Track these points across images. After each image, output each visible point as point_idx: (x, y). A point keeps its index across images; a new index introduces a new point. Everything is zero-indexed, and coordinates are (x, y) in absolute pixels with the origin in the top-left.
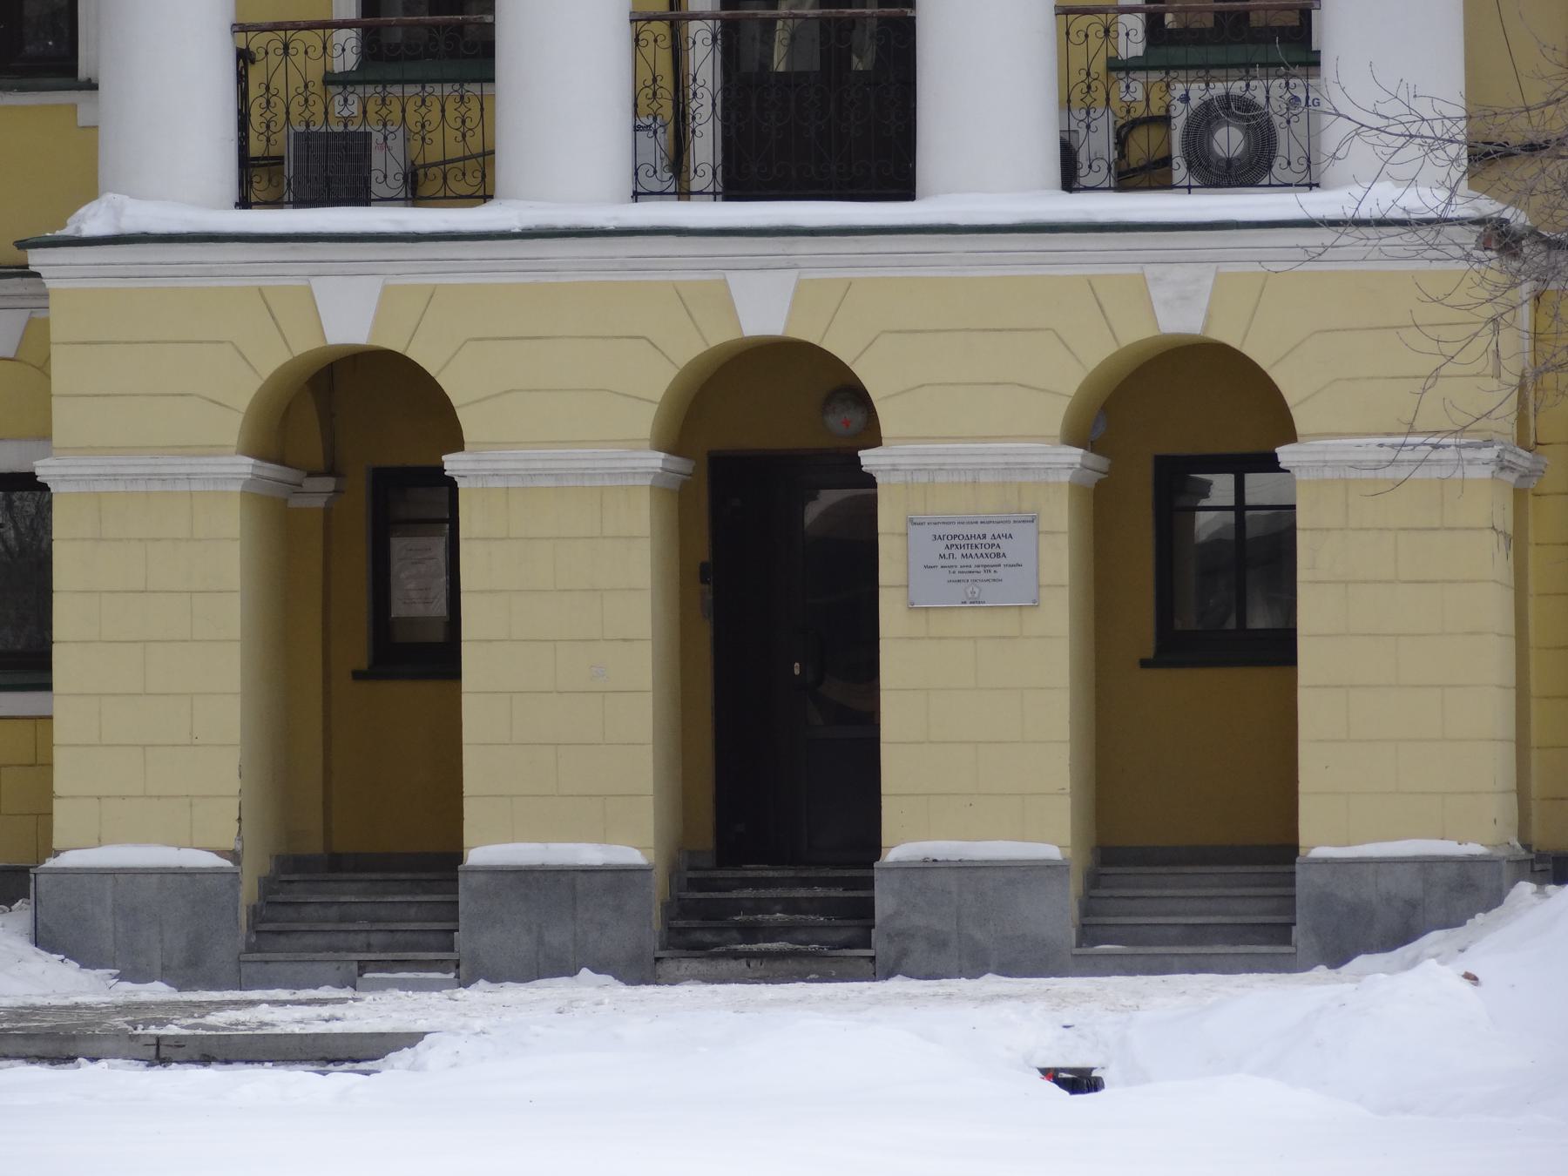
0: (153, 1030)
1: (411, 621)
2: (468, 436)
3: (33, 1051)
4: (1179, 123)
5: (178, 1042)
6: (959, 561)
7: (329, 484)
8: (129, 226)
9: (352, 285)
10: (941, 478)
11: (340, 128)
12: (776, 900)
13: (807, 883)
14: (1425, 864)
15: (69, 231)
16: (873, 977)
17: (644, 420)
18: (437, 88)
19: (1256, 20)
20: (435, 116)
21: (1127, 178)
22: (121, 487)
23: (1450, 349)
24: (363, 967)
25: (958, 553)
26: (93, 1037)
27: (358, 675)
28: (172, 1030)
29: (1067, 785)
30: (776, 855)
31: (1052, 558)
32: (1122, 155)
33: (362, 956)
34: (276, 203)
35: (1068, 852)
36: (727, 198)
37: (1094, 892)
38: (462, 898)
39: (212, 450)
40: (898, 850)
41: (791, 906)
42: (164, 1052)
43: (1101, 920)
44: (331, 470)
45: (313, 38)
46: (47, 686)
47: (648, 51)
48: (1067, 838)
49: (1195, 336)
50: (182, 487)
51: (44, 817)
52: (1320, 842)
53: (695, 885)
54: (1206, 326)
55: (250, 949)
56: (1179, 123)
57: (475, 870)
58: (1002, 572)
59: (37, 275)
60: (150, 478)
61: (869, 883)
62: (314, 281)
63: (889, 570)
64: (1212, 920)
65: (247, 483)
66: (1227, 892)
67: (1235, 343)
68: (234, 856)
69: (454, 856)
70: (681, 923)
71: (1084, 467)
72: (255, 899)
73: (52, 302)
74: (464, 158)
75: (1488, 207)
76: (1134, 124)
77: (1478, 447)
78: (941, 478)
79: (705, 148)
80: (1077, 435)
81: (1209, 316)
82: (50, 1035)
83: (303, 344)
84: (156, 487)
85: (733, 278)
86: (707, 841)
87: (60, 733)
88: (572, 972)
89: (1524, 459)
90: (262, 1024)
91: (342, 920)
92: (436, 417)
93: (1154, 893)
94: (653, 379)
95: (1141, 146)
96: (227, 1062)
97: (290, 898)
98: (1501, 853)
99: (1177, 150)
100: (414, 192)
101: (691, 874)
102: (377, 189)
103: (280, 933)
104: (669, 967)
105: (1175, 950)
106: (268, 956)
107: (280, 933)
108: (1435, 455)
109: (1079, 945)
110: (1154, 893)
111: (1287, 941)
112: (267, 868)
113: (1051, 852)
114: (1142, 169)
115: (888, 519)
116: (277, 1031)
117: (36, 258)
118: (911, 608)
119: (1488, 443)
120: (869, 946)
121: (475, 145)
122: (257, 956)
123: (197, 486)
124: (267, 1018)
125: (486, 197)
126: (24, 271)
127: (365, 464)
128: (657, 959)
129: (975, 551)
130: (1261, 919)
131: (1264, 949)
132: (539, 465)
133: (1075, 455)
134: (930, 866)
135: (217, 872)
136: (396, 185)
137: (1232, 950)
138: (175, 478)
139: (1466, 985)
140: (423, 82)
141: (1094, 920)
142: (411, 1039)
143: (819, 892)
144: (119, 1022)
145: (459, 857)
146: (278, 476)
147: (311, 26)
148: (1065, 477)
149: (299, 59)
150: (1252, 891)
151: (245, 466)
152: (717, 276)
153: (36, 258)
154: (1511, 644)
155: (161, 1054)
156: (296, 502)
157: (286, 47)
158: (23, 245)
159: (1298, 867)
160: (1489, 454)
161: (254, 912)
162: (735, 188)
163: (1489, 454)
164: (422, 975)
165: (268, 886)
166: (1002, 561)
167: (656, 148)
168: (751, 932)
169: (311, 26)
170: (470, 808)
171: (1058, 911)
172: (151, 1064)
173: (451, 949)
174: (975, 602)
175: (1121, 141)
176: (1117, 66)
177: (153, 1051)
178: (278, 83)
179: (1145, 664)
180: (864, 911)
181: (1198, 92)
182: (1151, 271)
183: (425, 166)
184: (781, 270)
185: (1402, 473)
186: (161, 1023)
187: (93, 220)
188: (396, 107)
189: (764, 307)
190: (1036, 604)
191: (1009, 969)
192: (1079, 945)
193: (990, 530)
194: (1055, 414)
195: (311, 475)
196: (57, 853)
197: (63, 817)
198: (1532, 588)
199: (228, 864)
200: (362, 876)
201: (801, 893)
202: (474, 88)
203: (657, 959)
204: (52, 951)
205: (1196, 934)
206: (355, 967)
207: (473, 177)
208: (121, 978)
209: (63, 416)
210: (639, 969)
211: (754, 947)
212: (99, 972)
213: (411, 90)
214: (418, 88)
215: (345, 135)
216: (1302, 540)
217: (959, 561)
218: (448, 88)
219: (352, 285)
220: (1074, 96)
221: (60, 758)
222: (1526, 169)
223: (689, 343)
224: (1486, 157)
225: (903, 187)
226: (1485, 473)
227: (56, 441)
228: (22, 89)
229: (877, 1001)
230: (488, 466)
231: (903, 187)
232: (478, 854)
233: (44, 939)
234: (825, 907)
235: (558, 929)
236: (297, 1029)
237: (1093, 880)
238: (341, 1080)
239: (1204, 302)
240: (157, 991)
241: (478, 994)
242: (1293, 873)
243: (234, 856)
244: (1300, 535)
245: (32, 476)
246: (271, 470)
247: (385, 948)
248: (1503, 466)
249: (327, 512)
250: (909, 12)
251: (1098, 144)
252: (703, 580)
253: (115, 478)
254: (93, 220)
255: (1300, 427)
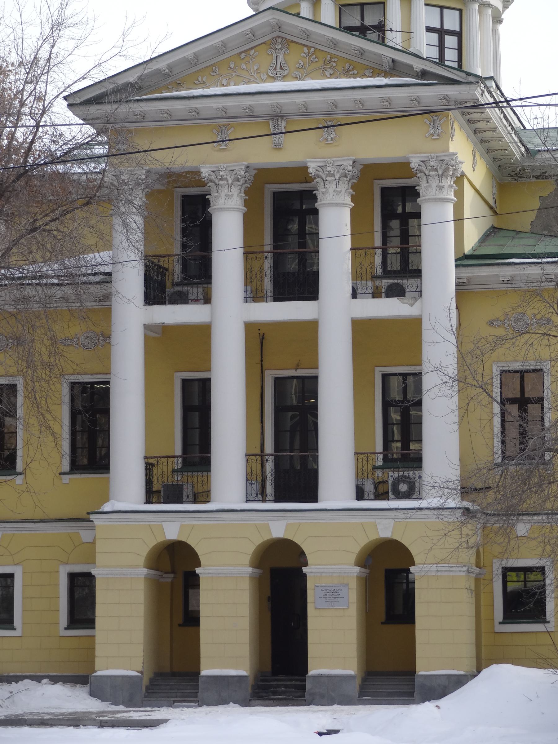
0: (101, 718)
1: (192, 611)
2: (202, 563)
3: (69, 723)
4: (390, 482)
5: (106, 722)
6: (328, 596)
7: (172, 575)
8: (116, 508)
9: (173, 524)
10: (324, 575)
11: (171, 483)
12: (282, 685)
13: (291, 680)
14: (449, 676)
15: (101, 510)
16: (306, 705)
17: (247, 559)
18: (196, 473)
19: (412, 456)
20: (195, 480)
21: (379, 496)
22: (113, 576)
23: (435, 542)
24: (174, 702)
25: (328, 594)
26: (86, 720)
27: (180, 625)
28: (106, 718)
29: (356, 655)
30: (282, 673)
31: (352, 596)
32: (376, 491)
33: (174, 699)
34: (159, 502)
35: (356, 673)
36: (275, 502)
37: (365, 683)
38: (200, 683)
39: (137, 567)
40: (312, 672)
41: (286, 686)
42: (103, 724)
43: (366, 691)
44: (173, 572)
45: (164, 460)
46: (94, 628)
47: (250, 464)
48: (356, 669)
49: (173, 540)
50: (129, 576)
51: (93, 662)
52: (422, 670)
53: (262, 681)
54: (392, 535)
55: (145, 697)
56: (390, 482)
57: (203, 677)
58: (339, 599)
59: (92, 521)
60: (121, 574)
61: (304, 680)
62: (163, 523)
63: (310, 599)
64: (395, 691)
65: (145, 575)
66: (400, 683)
67: (399, 540)
68: (141, 672)
69: (197, 673)
70: (257, 691)
71: (360, 572)
72: (148, 684)
73: (96, 528)
74: (203, 492)
75: (466, 504)
76: (380, 483)
77: (462, 567)
78: (324, 575)
79: (270, 489)
80: (358, 564)
81: (392, 533)
82: (74, 719)
83: (160, 539)
84: (122, 576)
85: (270, 522)
86: (268, 668)
87: (98, 639)
88: (227, 703)
89: (477, 570)
90: (130, 717)
91: (171, 689)
92: (300, 555)
93: (380, 683)
94: (249, 548)
95: (381, 489)
96: (119, 727)
97: (157, 683)
98: (468, 674)
99: (390, 490)
100: (195, 501)
101: (261, 678)
102: (185, 498)
103: (153, 693)
104: (253, 702)
105: (384, 698)
106: (150, 699)
107: (153, 693)
108: (451, 569)
109: (359, 697)
110: (380, 683)
111: (413, 696)
112: (152, 675)
113: (351, 672)
114: (382, 494)
115: (310, 585)
116: (132, 718)
117: (92, 517)
118: (316, 608)
119: (465, 566)
120: (304, 697)
121: (206, 488)
122: (147, 699)
123: (133, 576)
124: (131, 715)
125: (209, 501)
126: (89, 520)
127: (176, 569)
128: (250, 700)
129: (332, 594)
130: (408, 691)
131: (407, 698)
132: (220, 571)
133: (358, 569)
134: (320, 676)
135: (137, 677)
136: (191, 498)
137: (398, 698)
138: (127, 574)
139: (436, 709)
140: (193, 472)
141: (363, 691)
142: (165, 721)
143: (293, 683)
144: (93, 716)
145: (199, 673)
146: (160, 574)
147: (164, 457)
148: (355, 574)
149: (161, 466)
150: (405, 683)
151: (145, 571)
152: (373, 521)
153: (92, 517)
154: (474, 619)
155: (102, 725)
156: (161, 580)
157: (368, 459)
158: (89, 513)
159: (415, 677)
160: (465, 569)
161: (147, 688)
162: (277, 500)
163: (465, 569)
164: (189, 704)
165: (151, 680)
166: (339, 596)
167: (256, 487)
168: (275, 693)
169: (164, 457)
170: (202, 660)
171: (354, 688)
172: (99, 727)
173: (197, 697)
174: (332, 607)
175: (376, 487)
176: (375, 468)
177: (99, 724)
178: (365, 468)
179: (382, 623)
180: (303, 688)
181: (396, 475)
182: (378, 521)
183: (198, 493)
184: (282, 521)
185: (423, 574)
186: (103, 716)
187: (107, 507)
188: (186, 478)
189: (278, 530)
190: (348, 608)
191: (341, 703)
192: (359, 697)
193: (336, 588)
194: (352, 558)
195: (166, 573)
196: (96, 672)
197: (98, 662)
198: (482, 603)
199: (140, 674)
200: (175, 677)
201: (289, 683)
202: (205, 473)
203: (250, 700)
204: (94, 697)
205: (390, 694)
206: (172, 702)
207: (202, 496)
208: (112, 704)
209: (99, 558)
210: (245, 703)
211: (275, 697)
212: (106, 703)
213: (189, 474)
214: (191, 473)
215: (173, 485)
216: (416, 591)
217: (328, 596)
218: (199, 473)
219: (173, 524)
220: (360, 475)
221: (97, 647)
222: (473, 496)
223: (259, 540)
224: (465, 492)
225: (315, 499)
226: (464, 574)
227: (97, 564)
228: (81, 474)
229: (297, 711)
230: (207, 571)
231: (315, 499)
232: (204, 672)
233: (92, 694)
234: (295, 687)
235: (225, 692)
236: (137, 718)
237: (364, 680)
238: (146, 732)
239: (391, 528)
240: (121, 708)
241: (205, 709)
242: (414, 679)
243: (141, 672)
244: (416, 590)
245: (90, 573)
246: (152, 572)
247: (180, 697)
248: (468, 572)
249: (172, 583)
250: (209, 455)
251: (369, 487)
252: (269, 601)
253: (112, 574)
254: (107, 507)
255: (416, 562)
